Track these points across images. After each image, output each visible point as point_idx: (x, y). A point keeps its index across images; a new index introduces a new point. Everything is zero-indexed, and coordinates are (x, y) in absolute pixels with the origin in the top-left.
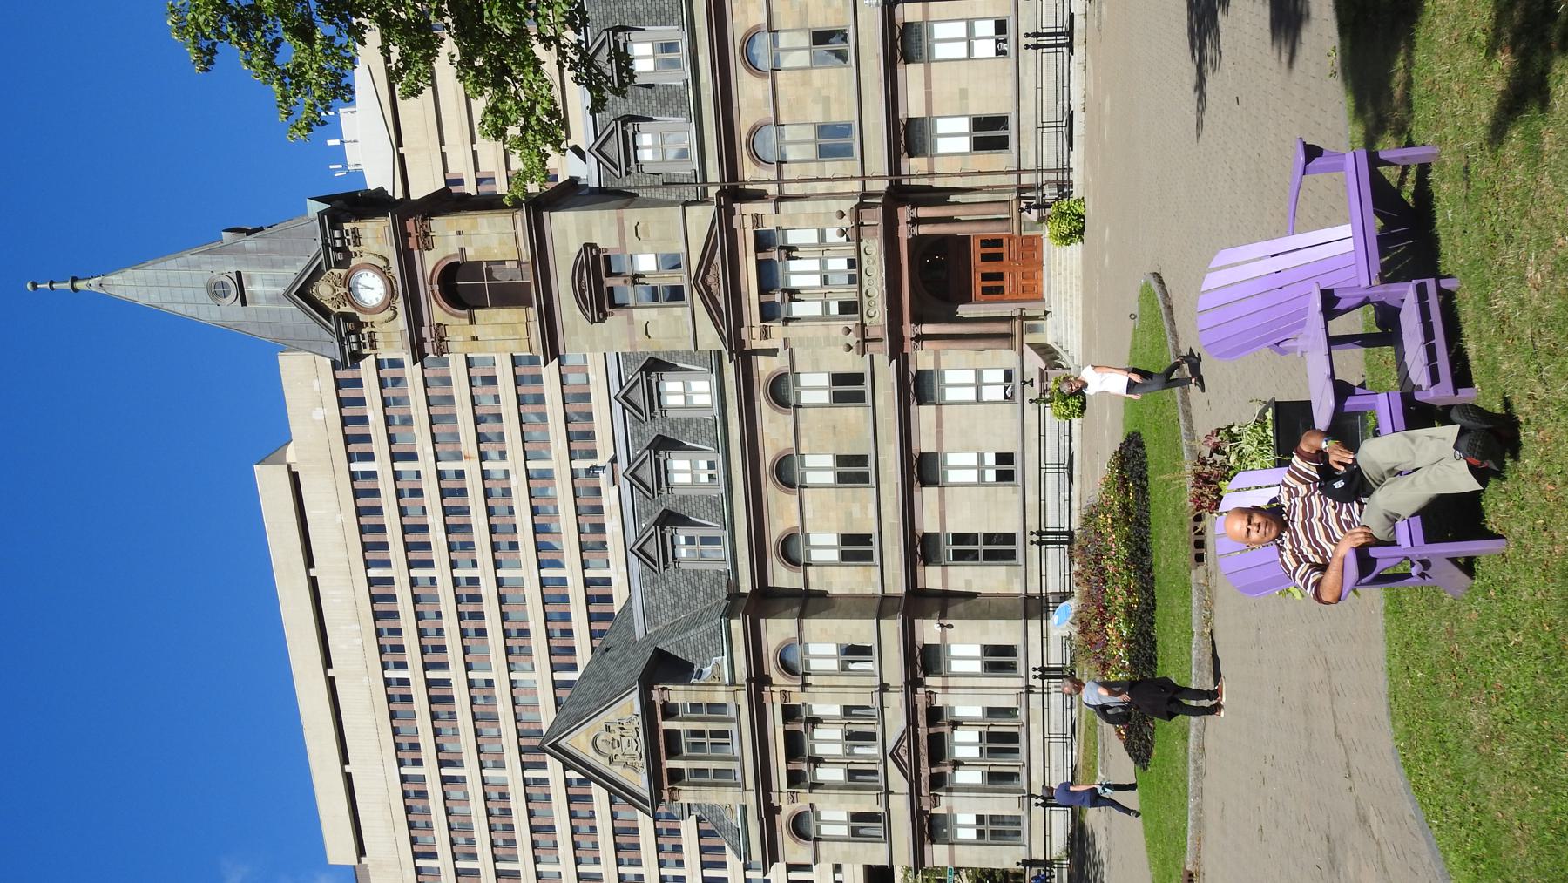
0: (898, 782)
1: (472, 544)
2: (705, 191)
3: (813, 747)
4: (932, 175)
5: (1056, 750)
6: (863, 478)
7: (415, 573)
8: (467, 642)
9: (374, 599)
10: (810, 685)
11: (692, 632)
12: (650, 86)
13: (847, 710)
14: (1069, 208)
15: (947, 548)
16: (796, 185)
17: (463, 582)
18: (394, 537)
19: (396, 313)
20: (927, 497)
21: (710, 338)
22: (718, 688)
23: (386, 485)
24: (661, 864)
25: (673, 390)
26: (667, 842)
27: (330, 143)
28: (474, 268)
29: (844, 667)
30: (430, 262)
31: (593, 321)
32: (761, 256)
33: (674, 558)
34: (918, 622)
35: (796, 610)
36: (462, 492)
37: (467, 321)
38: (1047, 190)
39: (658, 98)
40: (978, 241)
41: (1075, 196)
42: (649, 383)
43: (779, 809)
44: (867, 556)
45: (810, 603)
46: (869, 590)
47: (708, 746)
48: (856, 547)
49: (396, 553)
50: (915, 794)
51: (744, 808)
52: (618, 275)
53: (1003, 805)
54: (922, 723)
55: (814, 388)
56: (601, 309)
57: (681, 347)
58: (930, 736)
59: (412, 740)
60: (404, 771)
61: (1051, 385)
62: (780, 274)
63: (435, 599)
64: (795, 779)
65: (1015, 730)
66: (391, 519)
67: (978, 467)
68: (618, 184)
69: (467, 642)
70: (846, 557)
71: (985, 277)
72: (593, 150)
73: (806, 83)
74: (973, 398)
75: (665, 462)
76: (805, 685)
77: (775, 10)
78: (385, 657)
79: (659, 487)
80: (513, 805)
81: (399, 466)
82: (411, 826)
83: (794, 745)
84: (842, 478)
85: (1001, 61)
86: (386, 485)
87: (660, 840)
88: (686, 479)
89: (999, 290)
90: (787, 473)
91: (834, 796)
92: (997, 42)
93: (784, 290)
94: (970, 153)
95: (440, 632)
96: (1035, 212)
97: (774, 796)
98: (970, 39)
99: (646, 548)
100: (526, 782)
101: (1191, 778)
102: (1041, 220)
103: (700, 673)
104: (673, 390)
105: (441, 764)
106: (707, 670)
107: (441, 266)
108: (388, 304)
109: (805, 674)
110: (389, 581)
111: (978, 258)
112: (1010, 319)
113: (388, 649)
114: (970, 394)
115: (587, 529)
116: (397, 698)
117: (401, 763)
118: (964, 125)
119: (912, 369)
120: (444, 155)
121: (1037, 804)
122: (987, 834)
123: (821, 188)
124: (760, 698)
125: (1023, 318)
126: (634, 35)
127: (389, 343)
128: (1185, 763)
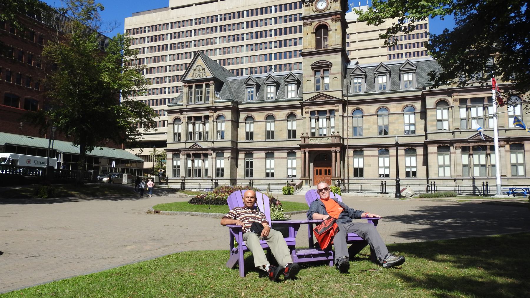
0: (188, 145)
1: (253, 39)
2: (346, 97)
3: (198, 123)
4: (348, 157)
5: (196, 186)
6: (268, 138)
7: (245, 23)
8: (227, 37)
9: (238, 12)
10: (214, 123)
11: (228, 92)
12: (374, 82)
13: (207, 132)
14: (339, 192)
15: (249, 160)
16: (346, 121)
17: (242, 36)
18: (255, 18)
19: (315, 12)
20: (263, 154)
21: (306, 97)
22: (213, 99)
23: (268, 16)
24: (169, 88)
25: (292, 87)
26: (175, 90)
27: (359, 3)
28: (326, 34)
29: (218, 132)
30: (328, 21)
31: (311, 66)
32: (328, 111)
33: (248, 88)
34: (230, 151)
35: (234, 120)
36: (266, 36)
37: (312, 32)
38: (343, 187)
39: (371, 84)
40: (330, 169)
41: (342, 193)
42: (294, 81)
43: (182, 114)
44: (247, 139)
45: (235, 123)
46: (238, 139)
47: (198, 96)
48: (250, 136)
49: (251, 18)
50: (185, 150)
51: (182, 105)
52: (324, 73)
53: (182, 172)
54: (204, 152)
55: (292, 125)
56: (315, 68)
57: (304, 89)
58: (200, 154)
59: (201, 22)
60: (194, 20)
61: (292, 186)
62: (323, 116)
63: (238, 29)
64: (189, 118)
65: (202, 176)
66: (259, 17)
67: (270, 168)
68: (348, 73)
69: (227, 37)
70: (247, 133)
71: (320, 170)
72: (358, 66)
73: (374, 124)
74: (289, 167)
75: (273, 85)
76: (214, 121)
77: (394, 115)
78: (223, 15)
79: (267, 84)
80: (184, 49)
81: (273, 19)
82: (179, 22)
83: (198, 118)
84: (268, 132)
85: (378, 175)
86: (268, 16)
87: (175, 88)
88: (269, 91)
89: (317, 174)
90: (270, 118)
91: (185, 129)
92: (383, 175)
93: (318, 117)
94: (354, 167)
95: (230, 30)
96: (338, 183)
97: (185, 113)
98: (384, 167)
99: (250, 80)
100: (190, 53)
101: (185, 212)
102: (336, 185)
103: (217, 94)
104: (292, 87)
105: (195, 30)
106: (218, 96)
107: (326, 24)
108: (317, 10)
109: (217, 122)
110: (243, 17)
111: (326, 169)
112: (309, 177)
113: (225, 16)
114: (289, 166)
115: (256, 69)
116: (212, 18)
117: (196, 19)
118: (361, 165)
119: (296, 151)
120: (355, 33)
121: (182, 181)
122: (175, 168)
123: (346, 127)
124: (211, 109)
125: (309, 180)
126: (388, 77)
127: (307, 10)
128: (189, 211)
